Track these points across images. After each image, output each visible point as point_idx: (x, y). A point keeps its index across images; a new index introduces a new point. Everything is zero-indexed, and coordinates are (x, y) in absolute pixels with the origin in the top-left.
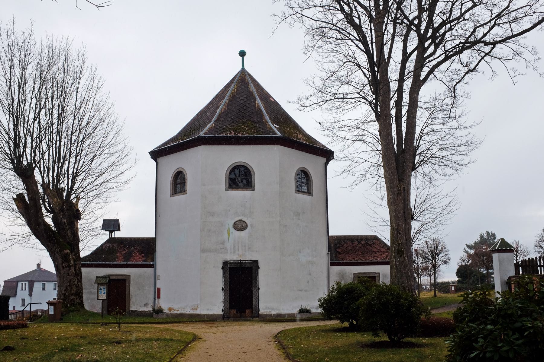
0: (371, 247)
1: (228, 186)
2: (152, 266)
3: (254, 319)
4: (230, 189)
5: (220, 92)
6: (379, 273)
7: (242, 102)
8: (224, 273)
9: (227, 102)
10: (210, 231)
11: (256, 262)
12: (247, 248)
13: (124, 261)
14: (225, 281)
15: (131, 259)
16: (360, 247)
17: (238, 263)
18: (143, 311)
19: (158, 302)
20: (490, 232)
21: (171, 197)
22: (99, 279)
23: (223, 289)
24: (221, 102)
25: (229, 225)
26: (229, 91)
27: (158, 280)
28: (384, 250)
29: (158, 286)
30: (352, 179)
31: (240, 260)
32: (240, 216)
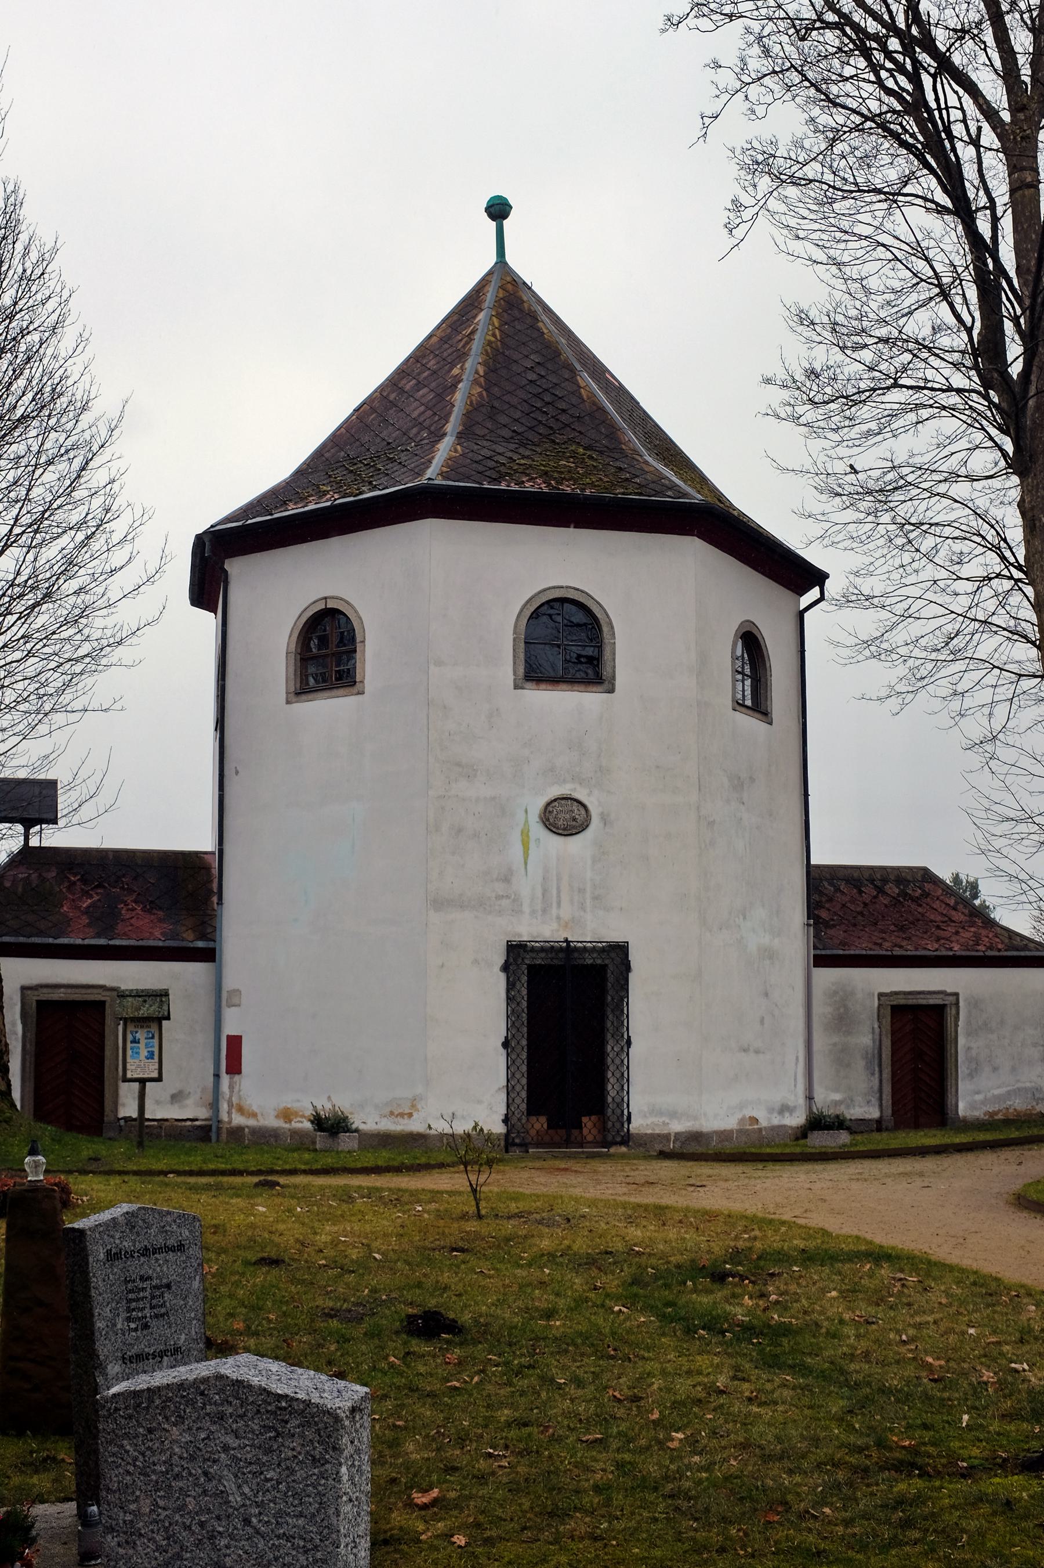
0: (920, 906)
1: (521, 670)
2: (209, 955)
3: (612, 1150)
4: (529, 685)
5: (430, 337)
6: (957, 995)
7: (532, 376)
8: (510, 986)
9: (482, 373)
10: (460, 830)
11: (619, 951)
12: (588, 895)
13: (98, 936)
14: (512, 1015)
15: (120, 928)
16: (886, 906)
17: (561, 949)
18: (167, 1120)
19: (231, 1087)
20: (963, 877)
21: (288, 702)
22: (130, 999)
23: (506, 1044)
24: (456, 371)
25: (526, 811)
26: (473, 332)
27: (229, 1006)
28: (962, 918)
29: (230, 1029)
30: (891, 674)
31: (566, 941)
32: (564, 781)
